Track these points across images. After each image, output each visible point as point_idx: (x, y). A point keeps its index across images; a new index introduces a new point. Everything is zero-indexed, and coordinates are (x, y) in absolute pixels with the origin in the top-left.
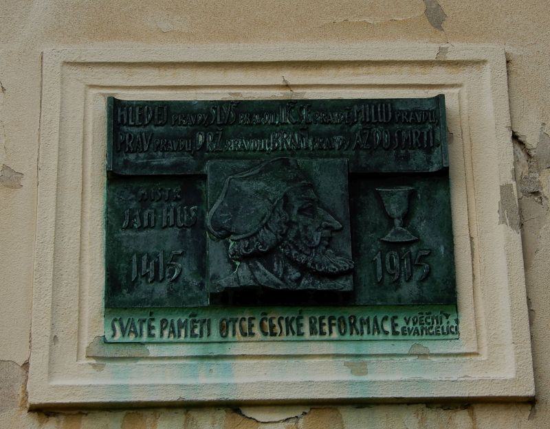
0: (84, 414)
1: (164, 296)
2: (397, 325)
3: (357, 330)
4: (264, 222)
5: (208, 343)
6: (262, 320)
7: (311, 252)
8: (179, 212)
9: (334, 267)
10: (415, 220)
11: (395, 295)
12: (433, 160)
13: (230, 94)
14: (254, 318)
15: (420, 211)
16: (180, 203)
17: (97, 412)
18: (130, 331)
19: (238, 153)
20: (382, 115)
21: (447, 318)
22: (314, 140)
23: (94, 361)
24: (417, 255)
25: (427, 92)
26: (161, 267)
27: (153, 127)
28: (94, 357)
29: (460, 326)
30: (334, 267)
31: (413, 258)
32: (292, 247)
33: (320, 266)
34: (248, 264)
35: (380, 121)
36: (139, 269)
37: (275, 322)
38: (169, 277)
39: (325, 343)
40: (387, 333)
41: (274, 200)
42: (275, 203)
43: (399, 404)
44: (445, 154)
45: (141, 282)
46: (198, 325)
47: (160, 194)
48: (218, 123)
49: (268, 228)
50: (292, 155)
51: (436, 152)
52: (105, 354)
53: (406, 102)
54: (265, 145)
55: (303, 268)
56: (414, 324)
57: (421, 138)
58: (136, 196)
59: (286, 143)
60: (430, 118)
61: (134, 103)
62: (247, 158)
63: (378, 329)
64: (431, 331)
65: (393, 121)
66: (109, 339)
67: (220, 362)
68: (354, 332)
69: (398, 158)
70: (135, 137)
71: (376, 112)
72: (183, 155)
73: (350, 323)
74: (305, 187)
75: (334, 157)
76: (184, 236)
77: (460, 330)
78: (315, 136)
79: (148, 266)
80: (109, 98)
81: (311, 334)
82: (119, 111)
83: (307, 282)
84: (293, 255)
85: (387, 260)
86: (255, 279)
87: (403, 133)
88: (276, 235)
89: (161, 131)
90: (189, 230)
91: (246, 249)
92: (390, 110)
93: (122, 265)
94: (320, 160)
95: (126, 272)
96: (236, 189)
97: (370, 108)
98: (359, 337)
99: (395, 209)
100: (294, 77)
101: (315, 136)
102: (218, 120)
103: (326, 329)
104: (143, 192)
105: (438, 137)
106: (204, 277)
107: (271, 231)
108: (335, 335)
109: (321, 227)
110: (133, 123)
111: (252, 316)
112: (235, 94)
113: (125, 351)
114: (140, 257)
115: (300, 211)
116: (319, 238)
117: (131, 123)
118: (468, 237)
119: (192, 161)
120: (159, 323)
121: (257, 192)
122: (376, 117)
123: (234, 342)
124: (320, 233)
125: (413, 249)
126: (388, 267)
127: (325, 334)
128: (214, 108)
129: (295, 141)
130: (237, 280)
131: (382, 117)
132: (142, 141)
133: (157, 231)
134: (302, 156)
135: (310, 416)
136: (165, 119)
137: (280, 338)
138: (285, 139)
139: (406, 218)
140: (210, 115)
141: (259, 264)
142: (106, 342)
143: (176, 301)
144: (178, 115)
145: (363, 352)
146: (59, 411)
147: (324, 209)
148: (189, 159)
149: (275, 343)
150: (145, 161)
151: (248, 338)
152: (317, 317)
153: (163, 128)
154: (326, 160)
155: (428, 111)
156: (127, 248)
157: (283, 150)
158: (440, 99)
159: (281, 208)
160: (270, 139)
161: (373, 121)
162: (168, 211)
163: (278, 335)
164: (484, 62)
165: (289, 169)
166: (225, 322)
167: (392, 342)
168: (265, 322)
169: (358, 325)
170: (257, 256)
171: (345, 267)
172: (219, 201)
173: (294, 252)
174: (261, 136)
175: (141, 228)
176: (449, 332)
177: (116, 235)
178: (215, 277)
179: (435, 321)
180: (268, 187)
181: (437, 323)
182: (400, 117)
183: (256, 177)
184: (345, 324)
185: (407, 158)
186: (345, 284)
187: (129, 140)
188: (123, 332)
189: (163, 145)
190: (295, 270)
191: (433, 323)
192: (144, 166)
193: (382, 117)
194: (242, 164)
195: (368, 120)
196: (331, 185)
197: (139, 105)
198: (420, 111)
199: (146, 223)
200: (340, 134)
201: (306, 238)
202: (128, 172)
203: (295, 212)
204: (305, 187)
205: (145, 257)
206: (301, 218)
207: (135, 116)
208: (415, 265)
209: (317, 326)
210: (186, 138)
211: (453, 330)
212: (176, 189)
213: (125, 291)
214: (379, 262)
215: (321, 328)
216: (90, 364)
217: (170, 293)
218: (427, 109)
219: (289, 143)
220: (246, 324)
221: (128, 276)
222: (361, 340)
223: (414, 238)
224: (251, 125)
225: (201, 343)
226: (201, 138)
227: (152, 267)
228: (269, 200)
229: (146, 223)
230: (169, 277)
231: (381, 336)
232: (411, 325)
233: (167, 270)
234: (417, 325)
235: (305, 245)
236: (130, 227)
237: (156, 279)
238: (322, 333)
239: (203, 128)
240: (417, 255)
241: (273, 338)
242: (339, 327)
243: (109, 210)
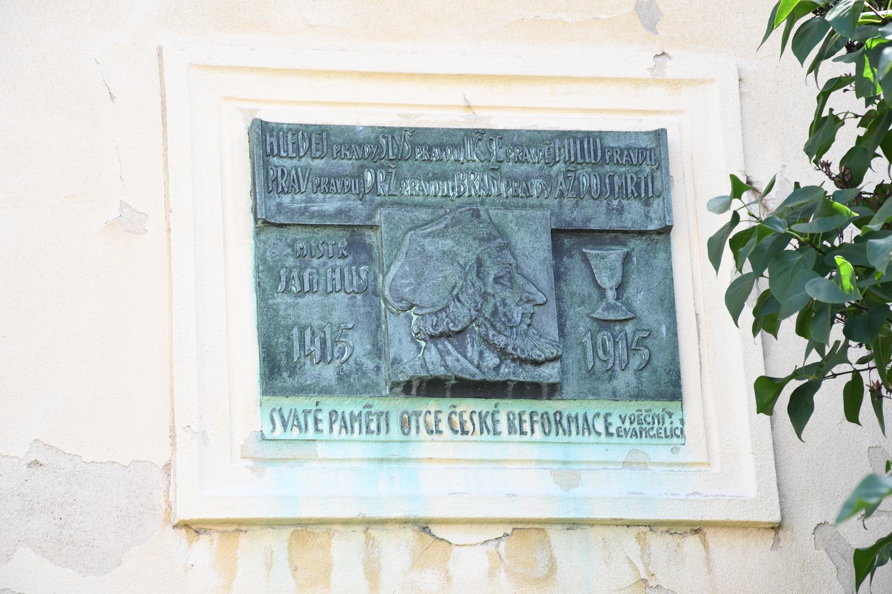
0: (241, 531)
1: (334, 382)
2: (610, 424)
3: (564, 430)
4: (455, 292)
5: (387, 442)
6: (451, 413)
7: (512, 333)
8: (346, 274)
9: (539, 352)
10: (630, 291)
11: (609, 387)
12: (652, 215)
13: (400, 115)
14: (440, 412)
15: (636, 281)
16: (347, 260)
17: (258, 528)
18: (293, 425)
19: (416, 198)
20: (589, 152)
21: (670, 417)
22: (508, 185)
23: (250, 463)
24: (634, 336)
25: (640, 120)
26: (329, 344)
27: (309, 160)
28: (251, 458)
29: (686, 428)
30: (539, 352)
31: (630, 341)
32: (488, 326)
33: (523, 351)
34: (436, 345)
35: (587, 160)
36: (302, 346)
37: (466, 417)
38: (338, 358)
39: (526, 445)
40: (599, 434)
41: (466, 264)
42: (467, 269)
43: (603, 525)
44: (668, 210)
45: (305, 364)
46: (375, 418)
47: (321, 249)
48: (391, 158)
49: (459, 301)
50: (482, 203)
51: (656, 203)
52: (264, 452)
53: (619, 137)
54: (448, 190)
55: (503, 353)
56: (631, 423)
57: (637, 186)
58: (293, 250)
59: (474, 187)
60: (648, 159)
61: (285, 126)
62: (428, 206)
63: (589, 429)
64: (652, 433)
65: (603, 162)
66: (268, 435)
67: (402, 465)
68: (561, 431)
69: (610, 210)
70: (289, 173)
71: (582, 148)
72: (348, 199)
73: (556, 420)
74: (501, 248)
75: (532, 207)
76: (354, 305)
77: (686, 433)
78: (510, 179)
79: (312, 342)
80: (254, 121)
81: (510, 433)
82: (268, 138)
83: (507, 370)
84: (490, 335)
85: (599, 342)
86: (446, 367)
87: (616, 178)
88: (469, 310)
89: (321, 166)
90: (359, 297)
91: (434, 327)
92: (599, 146)
93: (280, 340)
94: (517, 212)
95: (285, 349)
96: (419, 249)
97: (575, 143)
98: (566, 439)
99: (608, 282)
100: (477, 94)
101: (510, 179)
102: (391, 154)
103: (527, 427)
104: (301, 245)
105: (658, 185)
106: (380, 358)
107: (463, 304)
108: (538, 434)
109: (521, 300)
110: (285, 155)
111: (438, 409)
112: (405, 116)
113: (287, 451)
114: (302, 330)
115: (497, 280)
116: (520, 315)
117: (283, 154)
118: (694, 313)
119: (360, 206)
120: (328, 415)
121: (444, 253)
122: (583, 156)
123: (418, 441)
124: (520, 308)
125: (629, 328)
126: (600, 352)
127: (526, 433)
128: (383, 137)
129: (485, 186)
130: (424, 366)
131: (590, 156)
132: (298, 181)
133: (320, 298)
134: (493, 204)
135: (512, 538)
136: (325, 151)
137: (474, 438)
138: (473, 182)
139: (620, 288)
140: (377, 144)
141: (449, 346)
142: (263, 438)
143: (349, 383)
144: (341, 145)
145: (572, 458)
146: (211, 527)
147: (524, 277)
148: (353, 203)
149: (467, 444)
150: (303, 205)
151: (435, 436)
152: (517, 412)
153: (323, 161)
154: (524, 212)
155: (645, 149)
156: (285, 318)
157: (470, 196)
158: (660, 135)
159: (474, 276)
160: (454, 181)
161: (579, 160)
162: (333, 271)
163: (470, 433)
164: (712, 81)
165: (481, 223)
166: (406, 416)
167: (606, 447)
168: (453, 416)
169: (565, 422)
170: (447, 335)
171: (552, 353)
172: (398, 264)
173: (491, 333)
174: (444, 177)
175: (302, 293)
176: (673, 434)
177: (270, 302)
178: (396, 361)
179: (656, 420)
180: (457, 247)
181: (659, 423)
182: (611, 157)
183: (441, 234)
184: (549, 422)
185: (621, 211)
186: (549, 373)
187: (282, 178)
188: (285, 425)
189: (327, 183)
190: (492, 356)
191: (654, 423)
192: (303, 212)
193: (590, 156)
194: (423, 215)
195: (573, 159)
196: (532, 248)
197: (290, 130)
198: (635, 148)
199: (307, 288)
200: (540, 177)
201: (505, 315)
202: (281, 219)
203: (491, 279)
204: (501, 248)
205: (308, 332)
206: (498, 287)
207: (287, 145)
208: (631, 350)
209: (517, 422)
210: (352, 176)
211: (678, 432)
212: (342, 243)
213: (285, 375)
214: (589, 345)
215: (521, 426)
216: (247, 467)
217: (340, 379)
218: (643, 146)
219: (477, 187)
220: (431, 419)
221: (289, 355)
222: (568, 443)
223: (630, 315)
224: (430, 161)
225: (378, 441)
226: (369, 177)
227: (318, 343)
228: (458, 263)
229: (307, 288)
230: (338, 358)
231: (593, 438)
232: (627, 425)
233: (336, 349)
234: (635, 425)
235: (504, 323)
236: (287, 290)
237: (323, 358)
238: (522, 433)
239: (372, 164)
240: (634, 336)
241: (465, 437)
242: (543, 425)
243: (261, 268)
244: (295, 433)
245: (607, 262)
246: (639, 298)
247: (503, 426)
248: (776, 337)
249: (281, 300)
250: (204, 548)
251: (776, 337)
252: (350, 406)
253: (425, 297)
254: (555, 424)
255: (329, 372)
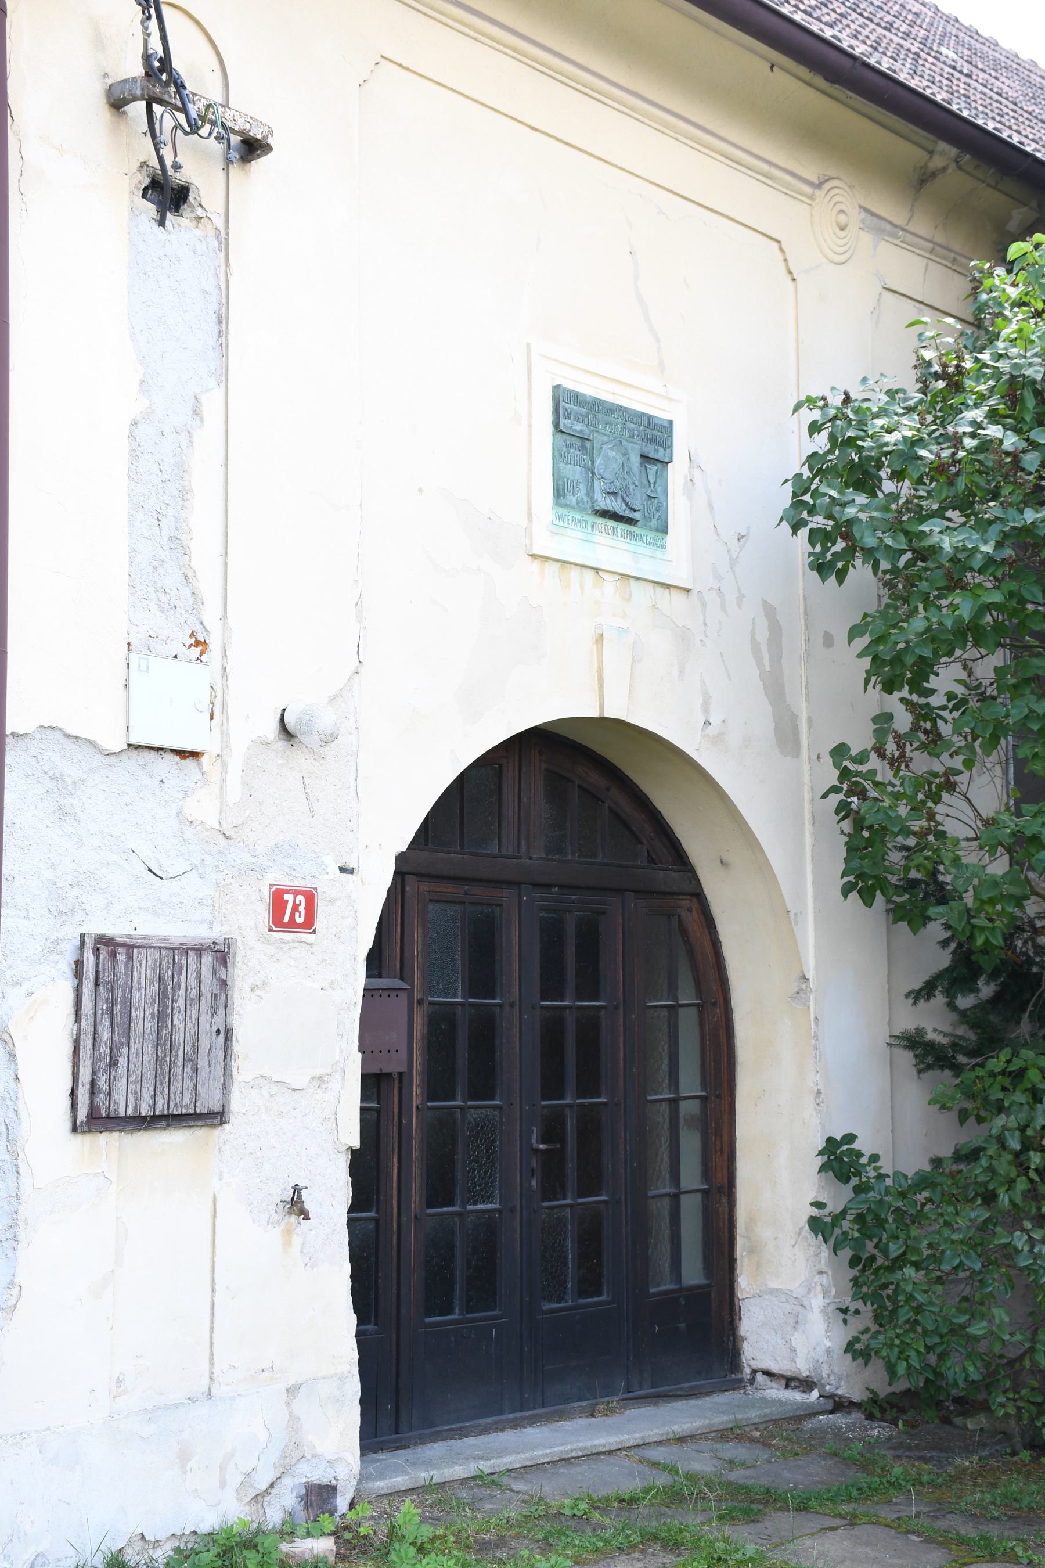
51: (668, 450)
139: (655, 484)
148: (585, 428)
175: (567, 464)
186: (637, 516)
192: (571, 428)
221: (564, 489)
231: (641, 544)
244: (562, 523)
245: (652, 469)
246: (659, 489)
247: (619, 534)
248: (765, 602)
249: (562, 465)
250: (537, 564)
251: (765, 602)
252: (578, 516)
253: (607, 475)
254: (633, 536)
255: (574, 500)
